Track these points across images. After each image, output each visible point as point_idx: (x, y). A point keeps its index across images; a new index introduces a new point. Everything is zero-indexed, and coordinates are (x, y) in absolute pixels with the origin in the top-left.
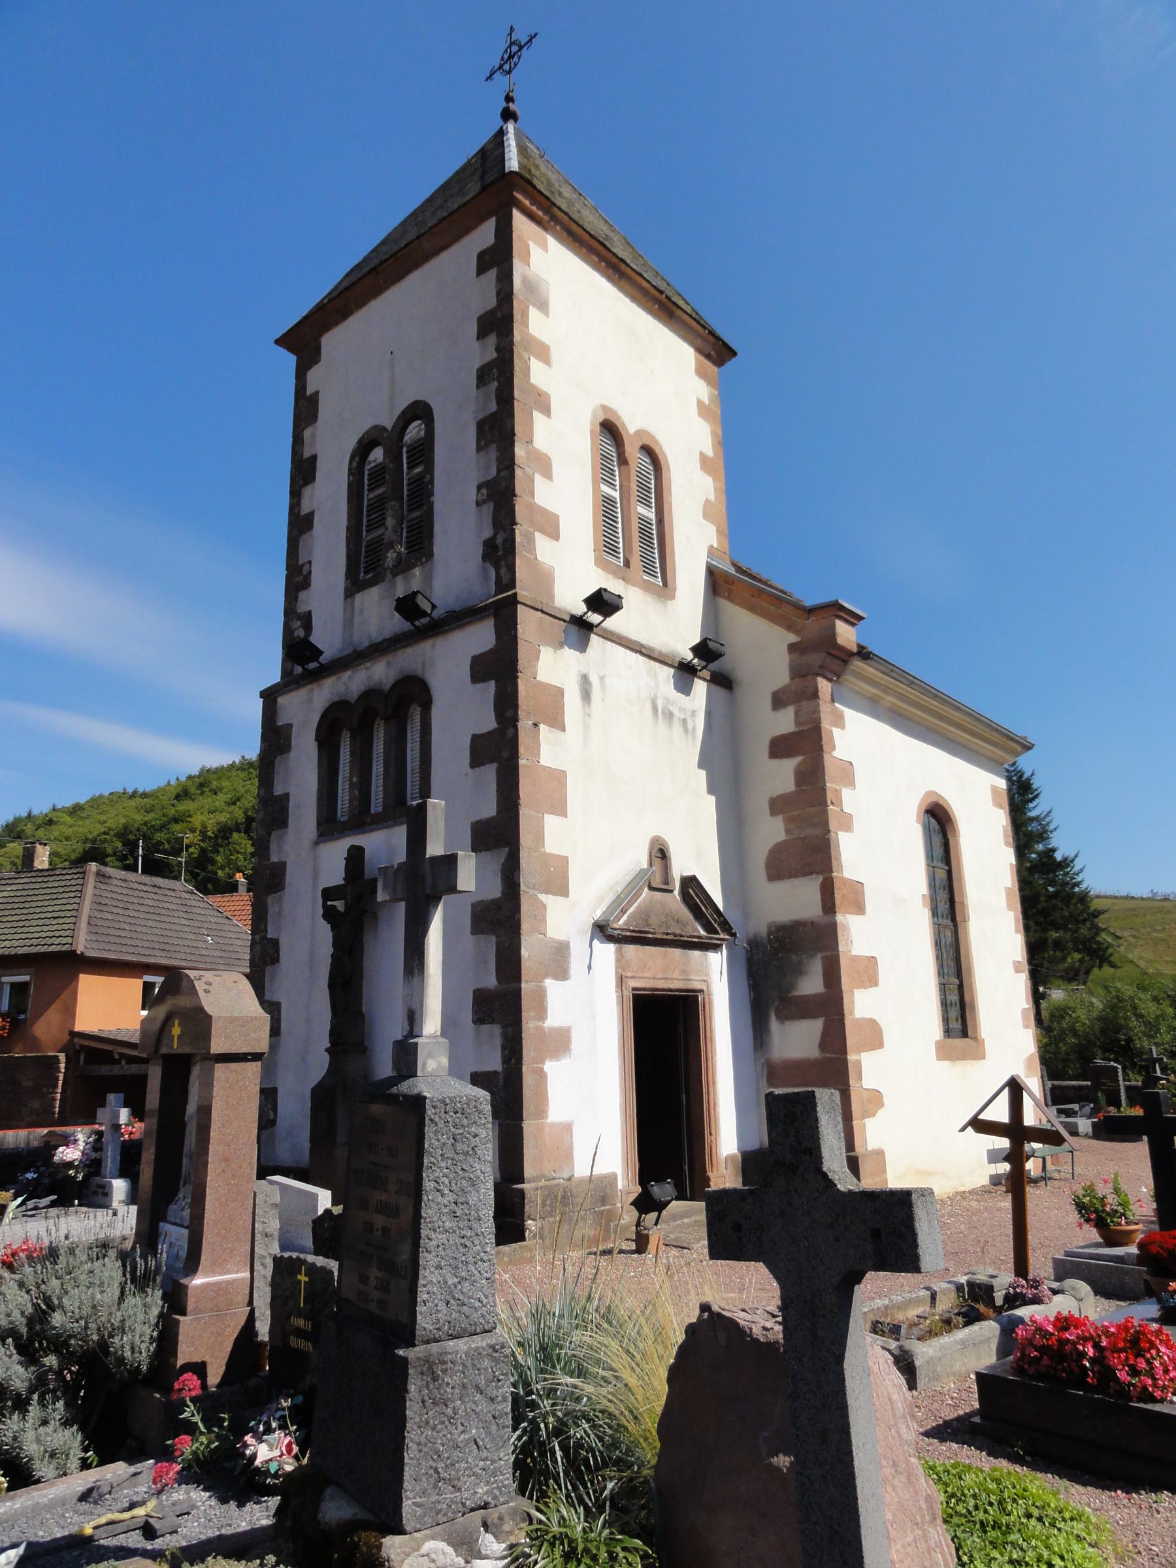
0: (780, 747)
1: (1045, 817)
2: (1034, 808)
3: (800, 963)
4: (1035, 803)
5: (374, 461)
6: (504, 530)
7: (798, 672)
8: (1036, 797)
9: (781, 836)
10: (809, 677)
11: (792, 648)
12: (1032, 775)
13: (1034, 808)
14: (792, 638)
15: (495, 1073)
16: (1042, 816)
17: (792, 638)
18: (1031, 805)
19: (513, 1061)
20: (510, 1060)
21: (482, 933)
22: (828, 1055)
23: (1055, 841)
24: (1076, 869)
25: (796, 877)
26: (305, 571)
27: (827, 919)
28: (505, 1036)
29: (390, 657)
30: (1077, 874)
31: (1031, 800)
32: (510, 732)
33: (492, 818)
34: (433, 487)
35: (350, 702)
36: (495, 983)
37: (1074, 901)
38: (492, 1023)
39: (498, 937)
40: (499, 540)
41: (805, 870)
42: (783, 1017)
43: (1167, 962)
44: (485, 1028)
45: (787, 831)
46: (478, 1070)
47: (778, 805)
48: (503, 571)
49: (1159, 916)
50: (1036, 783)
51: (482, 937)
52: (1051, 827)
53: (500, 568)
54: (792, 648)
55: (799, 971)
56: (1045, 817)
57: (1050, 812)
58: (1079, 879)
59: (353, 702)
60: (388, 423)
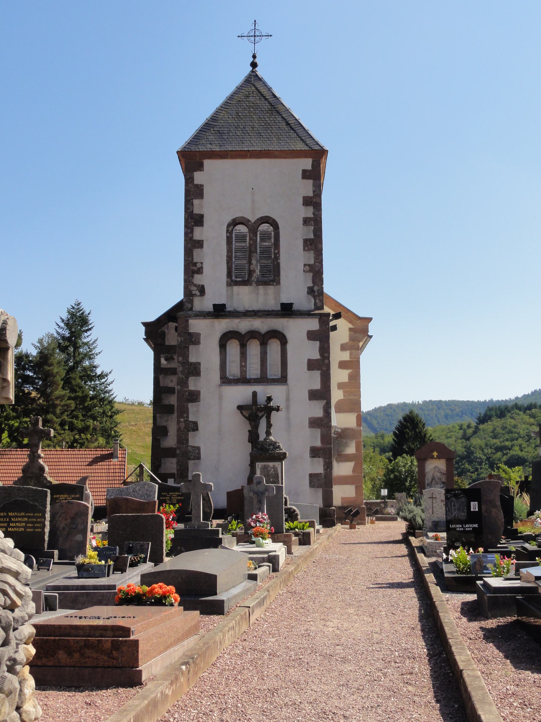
0: (343, 365)
1: (92, 344)
2: (88, 336)
3: (346, 443)
4: (89, 333)
5: (240, 230)
6: (318, 286)
7: (352, 339)
8: (90, 329)
9: (342, 397)
10: (357, 342)
11: (350, 329)
12: (89, 314)
13: (88, 336)
14: (351, 326)
15: (321, 474)
16: (91, 342)
17: (351, 326)
18: (86, 334)
19: (328, 470)
20: (327, 469)
21: (314, 427)
22: (355, 474)
23: (97, 361)
24: (108, 381)
25: (347, 412)
26: (199, 265)
27: (358, 428)
28: (325, 462)
29: (263, 320)
30: (109, 385)
31: (86, 331)
32: (326, 361)
33: (318, 390)
34: (279, 255)
35: (241, 334)
36: (320, 445)
37: (106, 403)
38: (319, 457)
39: (321, 429)
40: (316, 288)
41: (351, 410)
42: (338, 461)
43: (140, 446)
44: (316, 459)
45: (344, 396)
46: (312, 472)
47: (341, 386)
48: (317, 301)
49: (132, 416)
50: (92, 319)
51: (314, 429)
52: (97, 351)
53: (316, 299)
54: (350, 329)
55: (346, 445)
56: (92, 344)
57: (96, 340)
58: (110, 388)
59: (243, 334)
60: (253, 220)
